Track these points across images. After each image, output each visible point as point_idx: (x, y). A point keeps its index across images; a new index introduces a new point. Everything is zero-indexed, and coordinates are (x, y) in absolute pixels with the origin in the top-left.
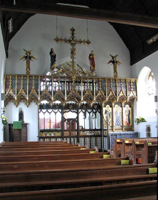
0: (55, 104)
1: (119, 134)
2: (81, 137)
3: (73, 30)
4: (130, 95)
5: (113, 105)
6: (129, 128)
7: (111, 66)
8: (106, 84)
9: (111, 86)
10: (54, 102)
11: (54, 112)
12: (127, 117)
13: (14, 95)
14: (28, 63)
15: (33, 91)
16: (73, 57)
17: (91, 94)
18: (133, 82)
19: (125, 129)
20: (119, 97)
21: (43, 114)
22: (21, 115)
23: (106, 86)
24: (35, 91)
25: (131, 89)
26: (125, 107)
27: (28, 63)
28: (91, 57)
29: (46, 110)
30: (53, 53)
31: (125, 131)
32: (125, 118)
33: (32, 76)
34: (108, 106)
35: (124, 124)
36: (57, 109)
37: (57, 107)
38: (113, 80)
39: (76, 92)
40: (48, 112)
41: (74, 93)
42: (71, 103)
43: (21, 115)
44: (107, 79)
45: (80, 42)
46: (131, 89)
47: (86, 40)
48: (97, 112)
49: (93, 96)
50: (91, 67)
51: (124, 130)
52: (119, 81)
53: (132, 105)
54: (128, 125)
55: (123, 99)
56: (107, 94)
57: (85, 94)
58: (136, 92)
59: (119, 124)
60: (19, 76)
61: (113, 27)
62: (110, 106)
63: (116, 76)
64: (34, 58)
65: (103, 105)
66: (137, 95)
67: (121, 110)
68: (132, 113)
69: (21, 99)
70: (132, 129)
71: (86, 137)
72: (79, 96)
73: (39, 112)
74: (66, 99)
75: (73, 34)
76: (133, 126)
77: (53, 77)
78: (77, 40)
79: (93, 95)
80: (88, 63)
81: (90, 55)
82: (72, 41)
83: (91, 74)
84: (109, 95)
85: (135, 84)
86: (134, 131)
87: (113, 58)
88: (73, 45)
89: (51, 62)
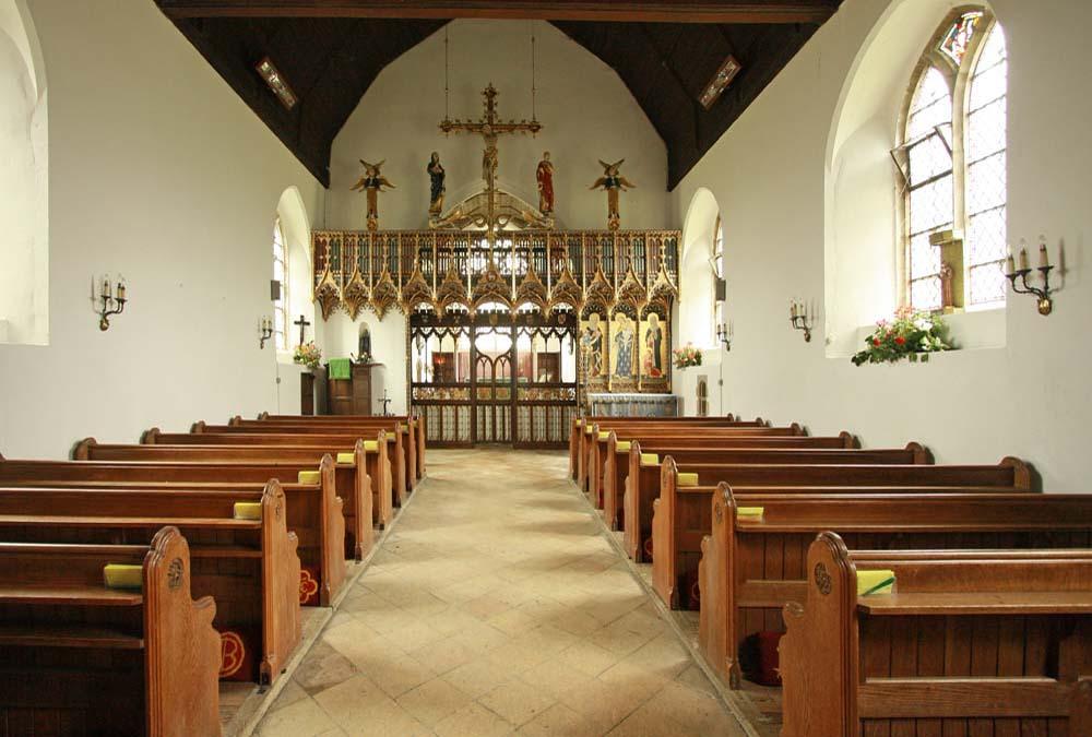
2: (520, 405)
3: (491, 93)
5: (610, 313)
7: (603, 195)
8: (616, 250)
10: (448, 307)
11: (451, 334)
12: (652, 350)
13: (338, 288)
14: (372, 200)
16: (489, 179)
17: (540, 281)
20: (652, 289)
22: (365, 342)
23: (616, 258)
26: (645, 319)
27: (372, 200)
31: (645, 392)
32: (645, 351)
33: (411, 236)
34: (594, 317)
35: (643, 371)
36: (489, 325)
40: (557, 333)
43: (365, 342)
44: (587, 236)
45: (511, 128)
48: (553, 334)
50: (541, 204)
51: (640, 388)
54: (654, 373)
55: (633, 294)
57: (523, 282)
58: (677, 274)
64: (627, 184)
65: (580, 314)
66: (677, 283)
67: (635, 329)
68: (664, 339)
69: (356, 300)
70: (666, 386)
71: (461, 405)
72: (506, 287)
74: (514, 296)
75: (490, 106)
76: (668, 377)
79: (546, 284)
80: (535, 188)
81: (541, 165)
82: (491, 127)
83: (542, 223)
85: (673, 248)
86: (670, 393)
87: (608, 168)
88: (490, 137)
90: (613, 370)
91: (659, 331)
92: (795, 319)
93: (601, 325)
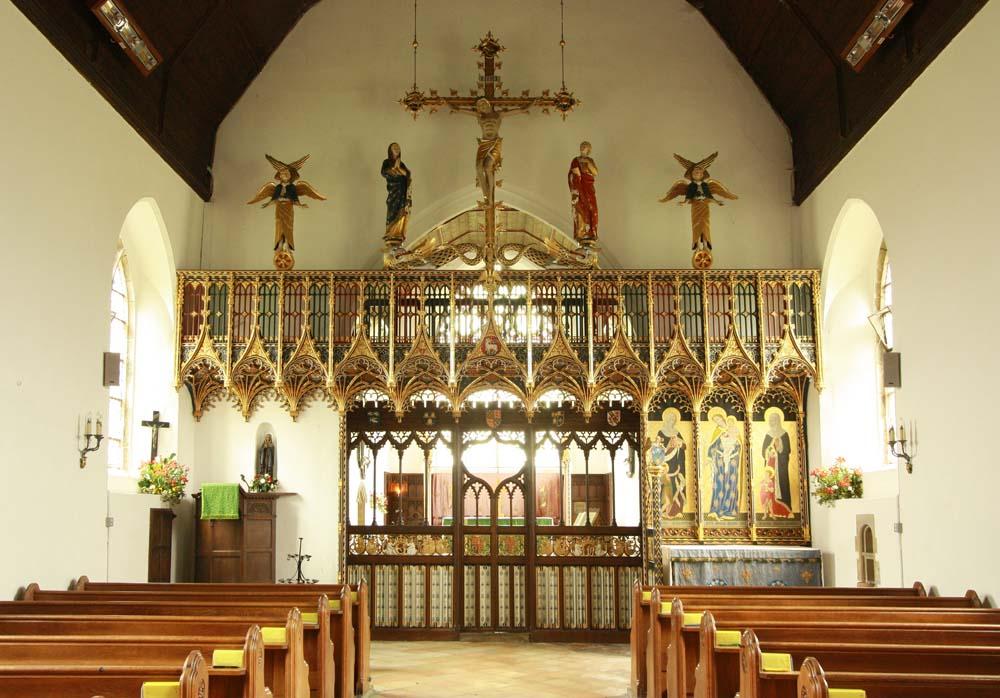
0: (419, 404)
1: (715, 558)
2: (541, 565)
3: (490, 49)
4: (776, 354)
5: (697, 408)
6: (785, 526)
7: (684, 210)
8: (706, 302)
9: (735, 312)
12: (775, 472)
15: (302, 345)
16: (487, 185)
18: (794, 286)
19: (761, 532)
20: (716, 367)
21: (396, 452)
22: (266, 456)
24: (312, 343)
25: (786, 327)
26: (759, 417)
28: (577, 171)
29: (383, 433)
30: (397, 165)
31: (763, 543)
32: (763, 475)
34: (671, 414)
37: (430, 422)
38: (690, 283)
39: (500, 346)
40: (368, 443)
41: (493, 354)
42: (431, 398)
43: (266, 456)
45: (525, 103)
46: (786, 327)
47: (554, 91)
49: (584, 366)
50: (576, 227)
51: (754, 537)
52: (745, 284)
53: (801, 409)
54: (778, 509)
56: (652, 352)
59: (728, 504)
60: (665, 279)
61: (701, 16)
62: (682, 412)
63: (704, 261)
66: (815, 356)
69: (252, 384)
70: (800, 534)
72: (517, 364)
73: (349, 446)
75: (489, 67)
76: (804, 517)
77: (280, 283)
78: (511, 96)
81: (575, 163)
83: (578, 259)
84: (667, 355)
85: (806, 297)
86: (809, 544)
87: (691, 168)
89: (390, 209)
90: (705, 506)
91: (785, 438)
92: (892, 443)
93: (684, 427)
